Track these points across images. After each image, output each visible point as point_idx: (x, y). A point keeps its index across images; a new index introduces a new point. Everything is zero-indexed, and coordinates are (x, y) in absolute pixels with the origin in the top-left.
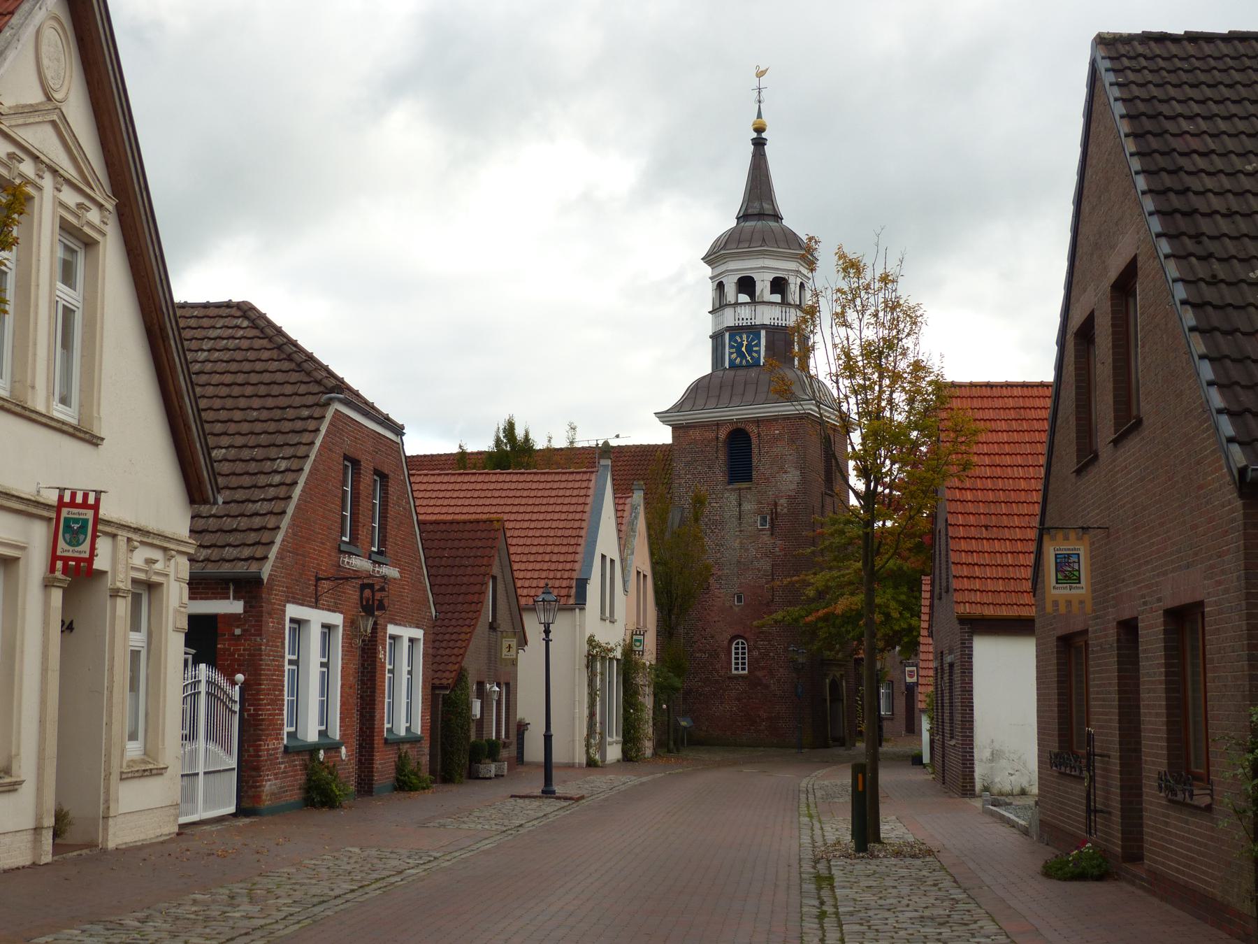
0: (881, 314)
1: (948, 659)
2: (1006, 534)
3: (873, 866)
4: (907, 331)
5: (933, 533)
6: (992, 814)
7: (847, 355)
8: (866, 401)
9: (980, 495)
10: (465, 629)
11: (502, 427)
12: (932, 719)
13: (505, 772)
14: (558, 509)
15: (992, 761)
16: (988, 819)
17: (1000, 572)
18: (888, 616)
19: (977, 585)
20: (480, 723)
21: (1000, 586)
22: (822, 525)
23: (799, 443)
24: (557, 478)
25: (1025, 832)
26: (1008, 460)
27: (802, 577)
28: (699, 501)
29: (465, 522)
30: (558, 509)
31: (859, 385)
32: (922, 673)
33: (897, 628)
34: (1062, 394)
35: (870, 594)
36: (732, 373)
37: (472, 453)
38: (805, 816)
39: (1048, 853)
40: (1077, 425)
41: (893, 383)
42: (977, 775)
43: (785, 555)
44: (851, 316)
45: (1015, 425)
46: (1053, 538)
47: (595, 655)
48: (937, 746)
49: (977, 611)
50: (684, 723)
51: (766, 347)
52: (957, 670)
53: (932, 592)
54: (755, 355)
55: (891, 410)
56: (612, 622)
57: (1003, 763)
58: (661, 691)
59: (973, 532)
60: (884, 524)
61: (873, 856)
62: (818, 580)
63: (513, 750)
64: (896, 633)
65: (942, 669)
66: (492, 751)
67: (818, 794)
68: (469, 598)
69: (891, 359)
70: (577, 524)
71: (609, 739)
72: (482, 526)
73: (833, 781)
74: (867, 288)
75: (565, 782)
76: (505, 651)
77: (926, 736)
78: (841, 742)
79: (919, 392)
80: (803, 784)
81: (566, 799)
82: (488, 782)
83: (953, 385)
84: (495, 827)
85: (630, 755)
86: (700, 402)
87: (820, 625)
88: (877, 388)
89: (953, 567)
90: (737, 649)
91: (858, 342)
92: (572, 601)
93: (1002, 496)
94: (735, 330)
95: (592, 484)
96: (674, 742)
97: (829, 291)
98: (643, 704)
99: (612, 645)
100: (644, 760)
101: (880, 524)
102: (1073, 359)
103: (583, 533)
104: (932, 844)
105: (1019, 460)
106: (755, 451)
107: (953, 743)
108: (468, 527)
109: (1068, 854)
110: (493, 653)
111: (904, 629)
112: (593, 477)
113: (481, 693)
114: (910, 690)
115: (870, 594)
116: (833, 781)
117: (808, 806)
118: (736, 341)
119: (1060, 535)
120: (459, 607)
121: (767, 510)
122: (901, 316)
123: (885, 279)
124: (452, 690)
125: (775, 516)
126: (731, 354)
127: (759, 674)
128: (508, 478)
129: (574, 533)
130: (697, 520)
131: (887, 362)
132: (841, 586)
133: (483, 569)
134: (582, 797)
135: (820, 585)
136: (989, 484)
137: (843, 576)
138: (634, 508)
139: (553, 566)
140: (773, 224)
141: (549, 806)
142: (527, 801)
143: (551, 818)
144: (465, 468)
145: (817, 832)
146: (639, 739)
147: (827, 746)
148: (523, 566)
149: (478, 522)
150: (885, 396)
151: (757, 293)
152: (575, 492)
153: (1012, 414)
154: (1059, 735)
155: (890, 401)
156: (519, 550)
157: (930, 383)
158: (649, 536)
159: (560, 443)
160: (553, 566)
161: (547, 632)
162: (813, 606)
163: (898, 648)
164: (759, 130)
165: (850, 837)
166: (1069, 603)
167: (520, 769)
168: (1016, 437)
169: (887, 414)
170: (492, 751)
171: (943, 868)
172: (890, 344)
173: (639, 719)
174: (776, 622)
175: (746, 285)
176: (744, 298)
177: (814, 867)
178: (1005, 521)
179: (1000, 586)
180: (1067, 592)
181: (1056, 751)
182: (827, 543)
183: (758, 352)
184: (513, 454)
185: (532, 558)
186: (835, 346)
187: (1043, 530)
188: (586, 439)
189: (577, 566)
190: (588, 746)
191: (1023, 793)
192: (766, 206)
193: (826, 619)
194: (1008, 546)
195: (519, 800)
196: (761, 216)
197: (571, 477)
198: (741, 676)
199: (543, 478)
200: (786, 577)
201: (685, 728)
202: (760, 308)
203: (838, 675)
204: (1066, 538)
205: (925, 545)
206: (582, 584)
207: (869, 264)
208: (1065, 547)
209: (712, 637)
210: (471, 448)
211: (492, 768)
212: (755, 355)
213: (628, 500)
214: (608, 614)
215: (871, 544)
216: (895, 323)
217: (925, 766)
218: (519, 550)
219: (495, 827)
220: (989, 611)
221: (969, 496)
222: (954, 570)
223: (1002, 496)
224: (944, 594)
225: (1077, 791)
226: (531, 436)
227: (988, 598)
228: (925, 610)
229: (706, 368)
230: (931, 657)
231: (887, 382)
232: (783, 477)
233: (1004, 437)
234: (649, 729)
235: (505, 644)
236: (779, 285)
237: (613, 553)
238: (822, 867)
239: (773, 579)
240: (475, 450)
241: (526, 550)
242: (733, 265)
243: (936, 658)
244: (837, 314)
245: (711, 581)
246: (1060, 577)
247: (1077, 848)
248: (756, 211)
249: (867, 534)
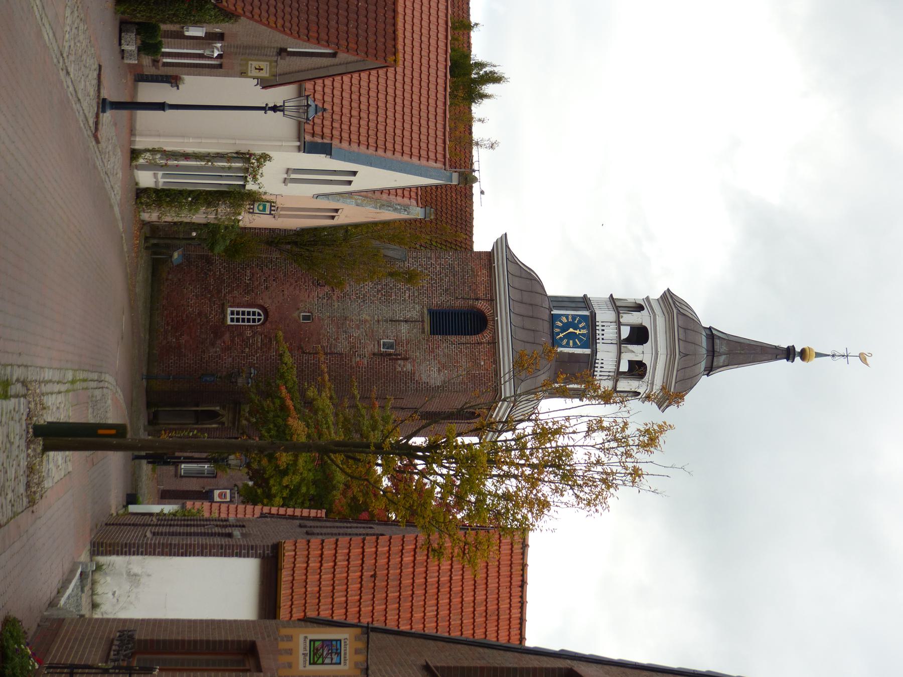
0: (599, 469)
1: (237, 533)
2: (367, 597)
3: (19, 442)
4: (581, 495)
5: (371, 520)
6: (72, 572)
7: (558, 431)
8: (509, 450)
9: (408, 571)
10: (280, 22)
11: (496, 69)
12: (174, 514)
13: (127, 61)
14: (407, 126)
15: (129, 574)
16: (67, 566)
17: (326, 589)
18: (284, 473)
19: (314, 565)
20: (180, 35)
21: (312, 588)
22: (383, 407)
23: (470, 385)
24: (440, 126)
25: (53, 604)
26: (444, 601)
27: (328, 384)
28: (411, 277)
29: (394, 25)
30: (407, 126)
31: (526, 443)
32: (224, 507)
33: (272, 482)
34: (509, 654)
35: (307, 448)
36: (546, 317)
37: (469, 37)
38: (74, 376)
39: (30, 625)
40: (475, 668)
41: (527, 479)
42: (114, 558)
43: (352, 368)
44: (599, 437)
45: (480, 609)
46: (357, 638)
47: (250, 161)
48: (147, 519)
49: (286, 563)
50: (176, 255)
51: (573, 354)
52: (224, 541)
53: (308, 518)
54: (565, 341)
55: (499, 476)
56: (285, 181)
57: (127, 587)
58: (211, 231)
59: (369, 562)
60: (378, 465)
61: (29, 443)
62: (324, 402)
63: (150, 70)
64: (267, 481)
65: (226, 526)
66: (150, 48)
67: (98, 393)
68: (313, 27)
69: (552, 477)
70: (389, 146)
71: (160, 173)
72: (390, 43)
73: (111, 406)
74: (628, 454)
75: (115, 124)
76: (255, 64)
77: (156, 509)
78: (153, 421)
79: (517, 506)
80: (108, 378)
81: (97, 124)
82: (116, 41)
83: (525, 546)
84: (67, 45)
85: (143, 197)
86: (517, 282)
87: (277, 401)
88: (522, 462)
89: (333, 539)
90: (254, 313)
91: (571, 443)
92: (308, 138)
93: (406, 593)
94: (591, 321)
95: (432, 163)
96: (156, 243)
97: (626, 415)
98: (197, 211)
99: (260, 180)
100: (137, 212)
101: (380, 462)
102: (545, 665)
103: (380, 152)
104: (41, 506)
105: (443, 612)
106: (464, 339)
107: (149, 534)
108: (390, 29)
109: (28, 644)
110: (252, 51)
111: (270, 489)
112: (439, 165)
113: (212, 37)
114: (207, 496)
115: (307, 448)
116: (111, 406)
117: (84, 380)
118: (580, 322)
119: (361, 645)
120: (303, 16)
121: (400, 349)
122: (595, 487)
123: (636, 473)
124: (215, 6)
125: (393, 358)
126: (567, 316)
127: (227, 337)
128: (441, 74)
129: (381, 143)
130: (391, 274)
131: (548, 475)
132: (317, 425)
133: (343, 43)
134: (98, 142)
135: (319, 403)
136: (419, 580)
137: (328, 428)
138: (406, 208)
139: (345, 119)
140: (703, 365)
141: (89, 106)
142: (95, 82)
143: (76, 107)
144: (454, 28)
145: (56, 388)
146: (159, 206)
147: (149, 405)
148: (346, 87)
149: (395, 39)
150: (513, 470)
151: (630, 347)
152: (424, 138)
153: (492, 607)
154: (152, 641)
155: (508, 476)
156: (364, 84)
157: (525, 518)
158: (375, 224)
159: (478, 132)
160: (345, 119)
161: (275, 109)
162: (297, 395)
163: (251, 483)
164: (803, 354)
165: (50, 419)
166: (290, 652)
167: (130, 78)
168: (468, 610)
169: (495, 472)
170: (150, 48)
171: (15, 514)
172: (568, 477)
173: (181, 206)
174: (281, 355)
175: (639, 335)
176: (625, 332)
177: (18, 380)
178: (380, 596)
179: (312, 588)
180: (301, 651)
181: (136, 637)
182: (364, 412)
183: (567, 345)
184: (466, 81)
185: (355, 97)
186: (568, 419)
187: (368, 630)
188: (480, 157)
189: (345, 145)
190: (153, 151)
191: (95, 606)
192: (722, 359)
193: (283, 408)
194: (353, 598)
195: (95, 74)
196: (712, 353)
197: (440, 141)
198: (225, 317)
199: (440, 111)
200: (329, 367)
201: (171, 256)
202: (614, 349)
203: (224, 419)
204: (357, 652)
205: (360, 512)
206: (326, 150)
207: (653, 457)
208: (347, 650)
209: (267, 288)
210: (476, 37)
211: (131, 47)
212: (565, 341)
213: (414, 202)
214: (293, 176)
215: (357, 449)
216: (589, 482)
217: (126, 507)
218: (364, 84)
219: (67, 45)
220: (285, 576)
221: (408, 559)
222: (329, 542)
223: (406, 593)
224: (305, 530)
225: (94, 657)
226: (486, 101)
227: (299, 575)
228: (290, 511)
229: (553, 288)
230: (240, 516)
231: (528, 471)
232: (435, 367)
233: (468, 598)
234: (170, 217)
235: (263, 65)
236: (637, 369)
237: (358, 184)
238: (18, 388)
239: (326, 354)
240: (473, 41)
241: (364, 91)
242: (661, 322)
243: (238, 520)
244: (601, 421)
245: (327, 289)
246: (317, 644)
247: (33, 654)
248: (717, 348)
249: (368, 446)
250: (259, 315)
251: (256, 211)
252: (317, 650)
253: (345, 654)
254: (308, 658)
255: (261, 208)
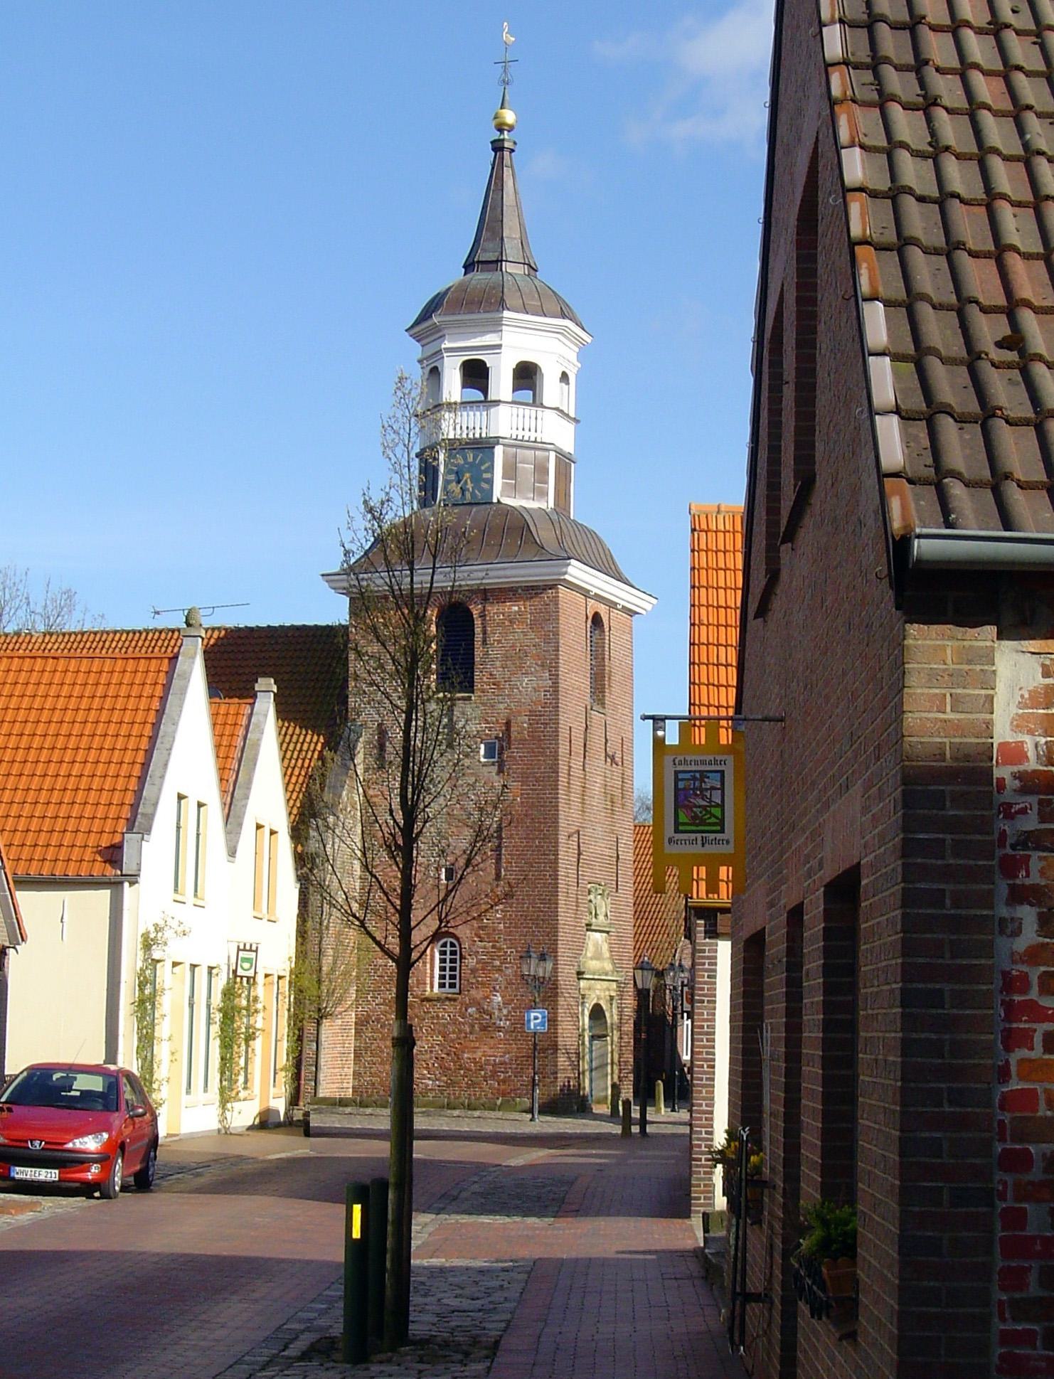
246: (683, 818)
250: (444, 945)
251: (251, 973)
252: (695, 817)
253: (703, 762)
254: (712, 836)
255: (246, 965)
